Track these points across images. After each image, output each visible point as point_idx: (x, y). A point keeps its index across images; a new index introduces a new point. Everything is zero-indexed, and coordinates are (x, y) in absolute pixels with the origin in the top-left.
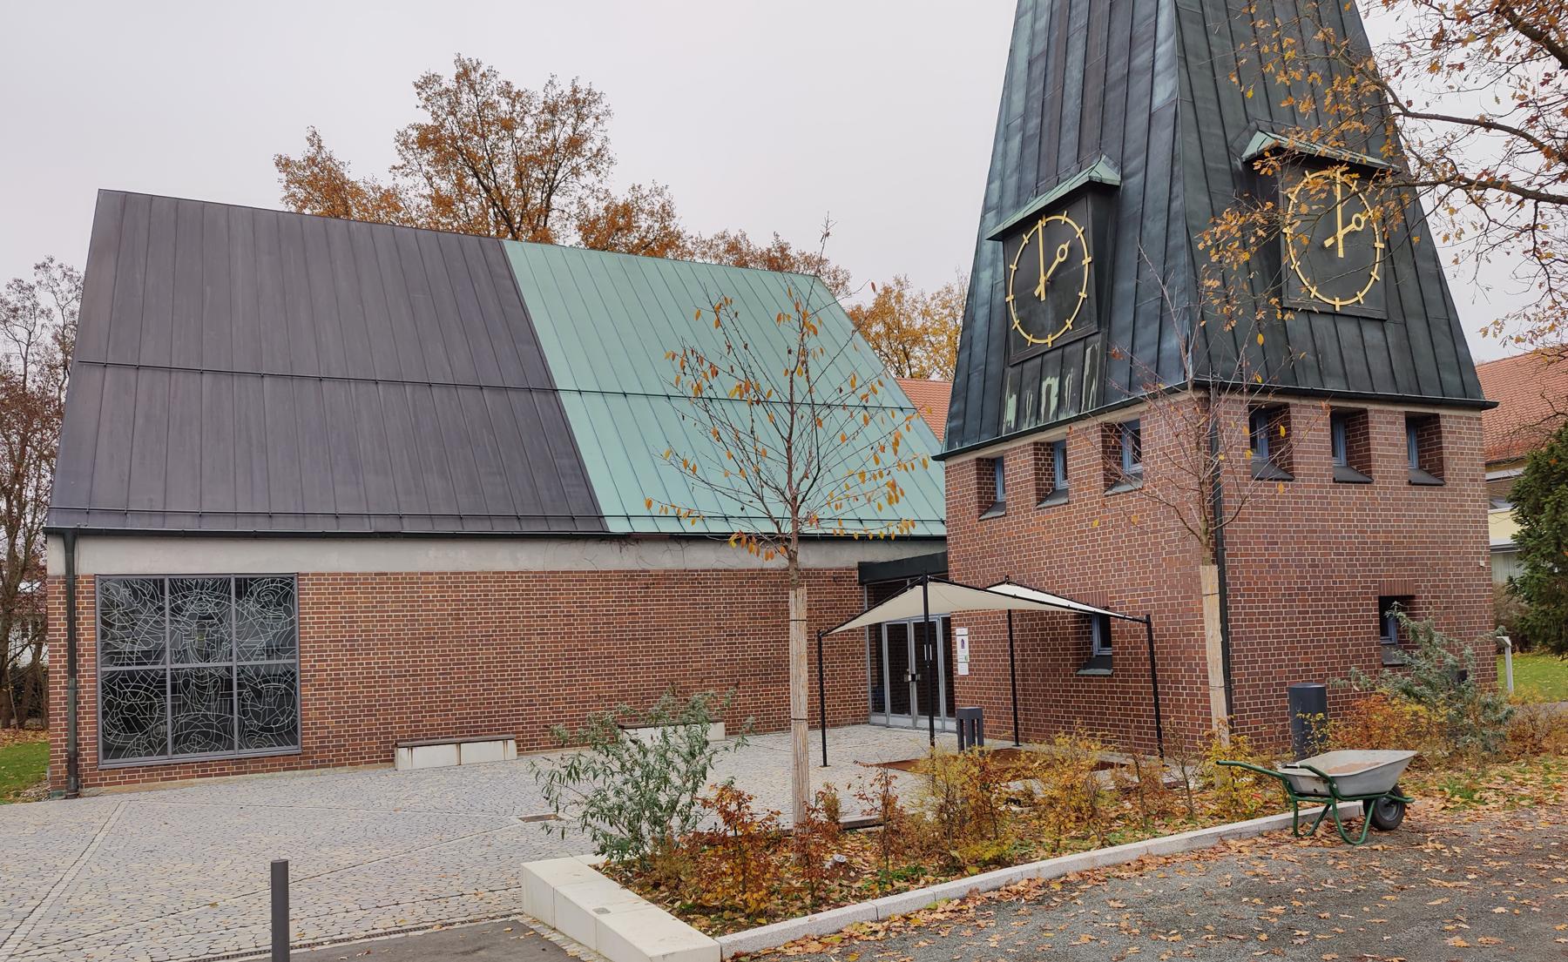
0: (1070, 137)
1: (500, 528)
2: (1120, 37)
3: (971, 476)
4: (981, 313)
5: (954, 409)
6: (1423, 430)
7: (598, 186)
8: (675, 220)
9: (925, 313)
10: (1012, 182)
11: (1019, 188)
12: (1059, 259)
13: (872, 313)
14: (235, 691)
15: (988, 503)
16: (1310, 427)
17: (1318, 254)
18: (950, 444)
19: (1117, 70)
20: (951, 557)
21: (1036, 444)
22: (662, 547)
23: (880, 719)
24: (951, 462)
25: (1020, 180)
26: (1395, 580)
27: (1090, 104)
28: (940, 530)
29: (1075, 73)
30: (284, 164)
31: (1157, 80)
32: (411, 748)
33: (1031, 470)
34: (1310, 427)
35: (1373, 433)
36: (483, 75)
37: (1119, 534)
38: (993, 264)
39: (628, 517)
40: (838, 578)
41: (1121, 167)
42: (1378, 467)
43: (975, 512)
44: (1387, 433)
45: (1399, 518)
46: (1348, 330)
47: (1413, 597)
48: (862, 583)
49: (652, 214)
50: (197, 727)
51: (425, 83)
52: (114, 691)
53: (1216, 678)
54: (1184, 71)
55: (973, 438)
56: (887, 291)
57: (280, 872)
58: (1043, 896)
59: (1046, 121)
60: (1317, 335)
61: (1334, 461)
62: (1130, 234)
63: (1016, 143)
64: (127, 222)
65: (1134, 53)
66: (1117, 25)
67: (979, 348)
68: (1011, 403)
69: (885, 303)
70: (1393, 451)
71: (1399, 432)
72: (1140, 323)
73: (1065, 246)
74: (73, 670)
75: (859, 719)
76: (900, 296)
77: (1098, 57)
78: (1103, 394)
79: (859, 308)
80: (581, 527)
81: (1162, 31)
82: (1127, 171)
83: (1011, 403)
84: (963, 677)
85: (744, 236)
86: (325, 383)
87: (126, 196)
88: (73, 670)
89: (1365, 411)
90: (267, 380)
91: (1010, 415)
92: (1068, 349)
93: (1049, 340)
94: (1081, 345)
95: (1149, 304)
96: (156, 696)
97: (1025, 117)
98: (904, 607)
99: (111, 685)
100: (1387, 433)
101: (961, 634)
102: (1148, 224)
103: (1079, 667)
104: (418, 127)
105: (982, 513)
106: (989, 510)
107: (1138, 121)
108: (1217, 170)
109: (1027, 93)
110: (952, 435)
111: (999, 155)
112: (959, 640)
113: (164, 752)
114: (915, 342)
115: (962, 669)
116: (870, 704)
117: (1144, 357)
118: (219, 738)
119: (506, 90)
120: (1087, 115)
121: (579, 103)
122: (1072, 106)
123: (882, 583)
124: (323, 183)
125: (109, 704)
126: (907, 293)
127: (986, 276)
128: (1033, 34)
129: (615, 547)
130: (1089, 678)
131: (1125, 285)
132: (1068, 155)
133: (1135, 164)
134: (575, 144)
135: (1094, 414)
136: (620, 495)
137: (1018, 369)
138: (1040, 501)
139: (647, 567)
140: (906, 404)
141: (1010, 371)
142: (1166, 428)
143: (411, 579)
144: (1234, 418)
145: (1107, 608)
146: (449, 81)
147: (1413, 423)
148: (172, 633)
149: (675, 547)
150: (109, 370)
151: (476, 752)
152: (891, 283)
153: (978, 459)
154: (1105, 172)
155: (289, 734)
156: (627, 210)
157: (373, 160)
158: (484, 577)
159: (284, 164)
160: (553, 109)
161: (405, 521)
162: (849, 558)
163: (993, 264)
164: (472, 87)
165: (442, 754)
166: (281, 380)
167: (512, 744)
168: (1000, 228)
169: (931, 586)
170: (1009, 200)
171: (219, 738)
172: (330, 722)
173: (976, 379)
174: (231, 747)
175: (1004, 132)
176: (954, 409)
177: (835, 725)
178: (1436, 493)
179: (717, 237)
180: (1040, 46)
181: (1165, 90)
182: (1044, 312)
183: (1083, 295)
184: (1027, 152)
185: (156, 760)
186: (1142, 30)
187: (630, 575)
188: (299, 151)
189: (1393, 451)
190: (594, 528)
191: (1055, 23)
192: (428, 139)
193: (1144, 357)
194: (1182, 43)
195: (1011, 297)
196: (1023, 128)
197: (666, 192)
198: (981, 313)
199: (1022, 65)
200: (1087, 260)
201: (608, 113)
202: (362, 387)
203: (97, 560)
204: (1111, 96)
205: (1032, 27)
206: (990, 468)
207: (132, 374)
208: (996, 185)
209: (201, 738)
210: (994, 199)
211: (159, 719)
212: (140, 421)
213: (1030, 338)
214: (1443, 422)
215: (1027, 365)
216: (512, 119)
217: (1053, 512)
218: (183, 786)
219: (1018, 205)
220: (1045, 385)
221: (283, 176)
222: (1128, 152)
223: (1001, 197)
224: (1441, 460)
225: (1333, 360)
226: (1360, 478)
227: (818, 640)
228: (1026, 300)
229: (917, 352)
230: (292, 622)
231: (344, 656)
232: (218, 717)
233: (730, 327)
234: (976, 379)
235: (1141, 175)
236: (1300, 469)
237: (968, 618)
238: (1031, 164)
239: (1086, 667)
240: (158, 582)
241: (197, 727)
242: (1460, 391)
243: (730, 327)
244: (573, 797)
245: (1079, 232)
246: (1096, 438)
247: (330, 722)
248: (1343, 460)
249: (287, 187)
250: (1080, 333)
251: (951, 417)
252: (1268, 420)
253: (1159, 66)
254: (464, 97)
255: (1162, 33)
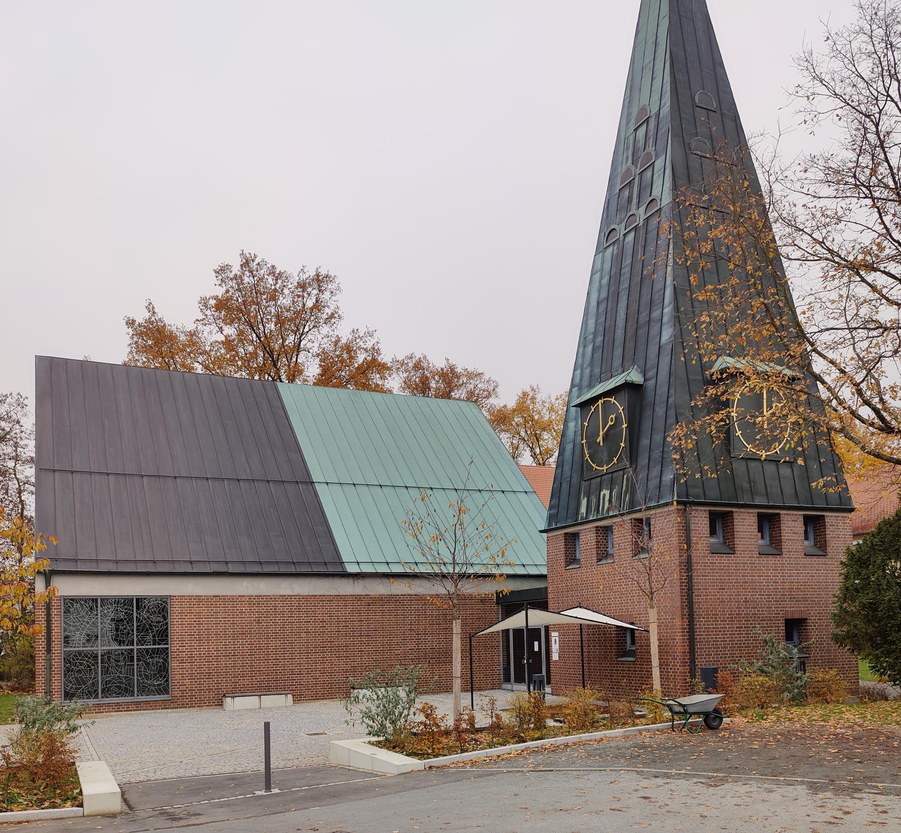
0: (618, 352)
1: (283, 569)
2: (645, 299)
3: (561, 543)
4: (569, 447)
5: (553, 502)
6: (814, 525)
7: (332, 333)
8: (381, 356)
9: (551, 409)
10: (587, 371)
11: (591, 377)
12: (610, 423)
13: (514, 411)
14: (135, 663)
15: (571, 559)
16: (745, 524)
17: (751, 429)
18: (550, 524)
19: (644, 317)
20: (549, 590)
21: (597, 527)
22: (378, 581)
23: (509, 686)
24: (551, 534)
25: (591, 371)
26: (794, 610)
27: (629, 334)
28: (544, 571)
29: (622, 315)
30: (131, 323)
31: (664, 327)
32: (233, 697)
33: (594, 542)
34: (745, 524)
35: (783, 527)
36: (258, 264)
37: (625, 589)
38: (576, 419)
39: (358, 563)
40: (483, 600)
41: (644, 373)
42: (786, 545)
43: (563, 564)
44: (792, 526)
45: (798, 575)
46: (770, 468)
47: (806, 619)
48: (498, 603)
49: (366, 350)
50: (114, 683)
51: (222, 270)
52: (70, 663)
53: (655, 662)
54: (677, 324)
55: (562, 519)
56: (525, 394)
57: (267, 725)
58: (555, 749)
59: (606, 339)
60: (751, 472)
61: (761, 542)
62: (648, 413)
63: (590, 348)
64: (54, 375)
65: (653, 309)
66: (644, 291)
67: (567, 468)
68: (584, 502)
69: (524, 402)
70: (795, 537)
71: (800, 527)
72: (651, 465)
73: (613, 416)
74: (49, 650)
75: (496, 686)
76: (533, 398)
77: (634, 308)
78: (632, 503)
79: (505, 406)
80: (331, 569)
81: (667, 301)
82: (647, 376)
83: (584, 502)
84: (556, 662)
85: (425, 357)
86: (178, 480)
87: (52, 359)
88: (49, 650)
89: (779, 514)
90: (145, 479)
91: (583, 510)
92: (615, 474)
93: (605, 468)
94: (621, 473)
95: (656, 454)
96: (93, 665)
97: (595, 334)
98: (516, 621)
99: (69, 660)
100: (792, 526)
101: (554, 635)
102: (657, 409)
103: (619, 656)
104: (216, 298)
105: (567, 565)
106: (571, 563)
107: (653, 349)
108: (695, 380)
109: (596, 321)
110: (551, 518)
111: (581, 355)
112: (553, 639)
113: (96, 697)
114: (544, 429)
115: (555, 657)
116: (502, 677)
117: (653, 483)
118: (127, 691)
119: (272, 271)
120: (627, 340)
121: (320, 280)
122: (620, 333)
123: (510, 604)
124: (154, 337)
125: (68, 670)
126: (539, 397)
127: (572, 425)
128: (600, 286)
129: (350, 581)
130: (623, 663)
131: (645, 442)
132: (617, 362)
133: (651, 373)
134: (318, 306)
135: (628, 513)
136: (353, 551)
137: (588, 483)
138: (599, 560)
139: (369, 593)
140: (529, 489)
141: (584, 484)
142: (665, 523)
143: (232, 599)
144: (700, 520)
145: (632, 624)
146: (236, 269)
147: (807, 520)
148: (102, 629)
149: (386, 581)
150: (57, 474)
151: (269, 701)
152: (528, 390)
153: (566, 534)
154: (635, 376)
155: (164, 689)
156: (348, 348)
157: (181, 315)
158: (274, 598)
159: (131, 323)
160: (302, 286)
161: (230, 565)
162: (489, 588)
163: (576, 419)
164: (251, 272)
165: (250, 702)
166: (153, 478)
167: (290, 696)
168: (578, 401)
169: (530, 612)
170: (585, 382)
171: (126, 690)
172: (187, 682)
173: (565, 486)
174: (133, 696)
175: (583, 342)
176: (553, 502)
177: (480, 690)
178: (821, 560)
179: (407, 358)
180: (604, 295)
181: (667, 334)
182: (602, 452)
183: (622, 445)
184: (595, 355)
185: (129, 699)
186: (656, 296)
187: (359, 598)
188: (141, 316)
189: (795, 537)
190: (339, 569)
191: (612, 282)
192: (222, 304)
193: (653, 483)
194: (677, 309)
195: (584, 441)
196: (594, 341)
197: (375, 334)
198: (569, 447)
199: (594, 304)
200: (625, 426)
201: (338, 289)
202: (199, 482)
203: (67, 587)
204: (640, 332)
205: (600, 282)
206: (572, 539)
207: (69, 475)
208: (578, 372)
209: (117, 690)
210: (577, 380)
211: (94, 678)
212: (78, 505)
213: (594, 466)
214: (827, 520)
215: (593, 481)
216: (275, 290)
217: (606, 567)
218: (107, 717)
219: (591, 386)
220: (602, 493)
221: (130, 330)
222: (648, 366)
223: (581, 380)
224: (825, 541)
225: (760, 487)
226: (776, 552)
227: (469, 639)
228: (592, 444)
229: (546, 435)
230: (167, 623)
231: (195, 644)
232: (126, 678)
233: (428, 501)
234: (565, 486)
235: (654, 380)
236: (739, 548)
237: (559, 627)
238: (598, 363)
239: (622, 656)
240: (95, 600)
241: (114, 683)
242: (838, 501)
243: (428, 501)
244: (356, 709)
245: (621, 409)
246: (628, 526)
247: (187, 682)
248: (768, 543)
249: (132, 338)
250: (621, 466)
251: (551, 507)
252: (721, 522)
253: (665, 319)
254: (246, 280)
255: (667, 301)
